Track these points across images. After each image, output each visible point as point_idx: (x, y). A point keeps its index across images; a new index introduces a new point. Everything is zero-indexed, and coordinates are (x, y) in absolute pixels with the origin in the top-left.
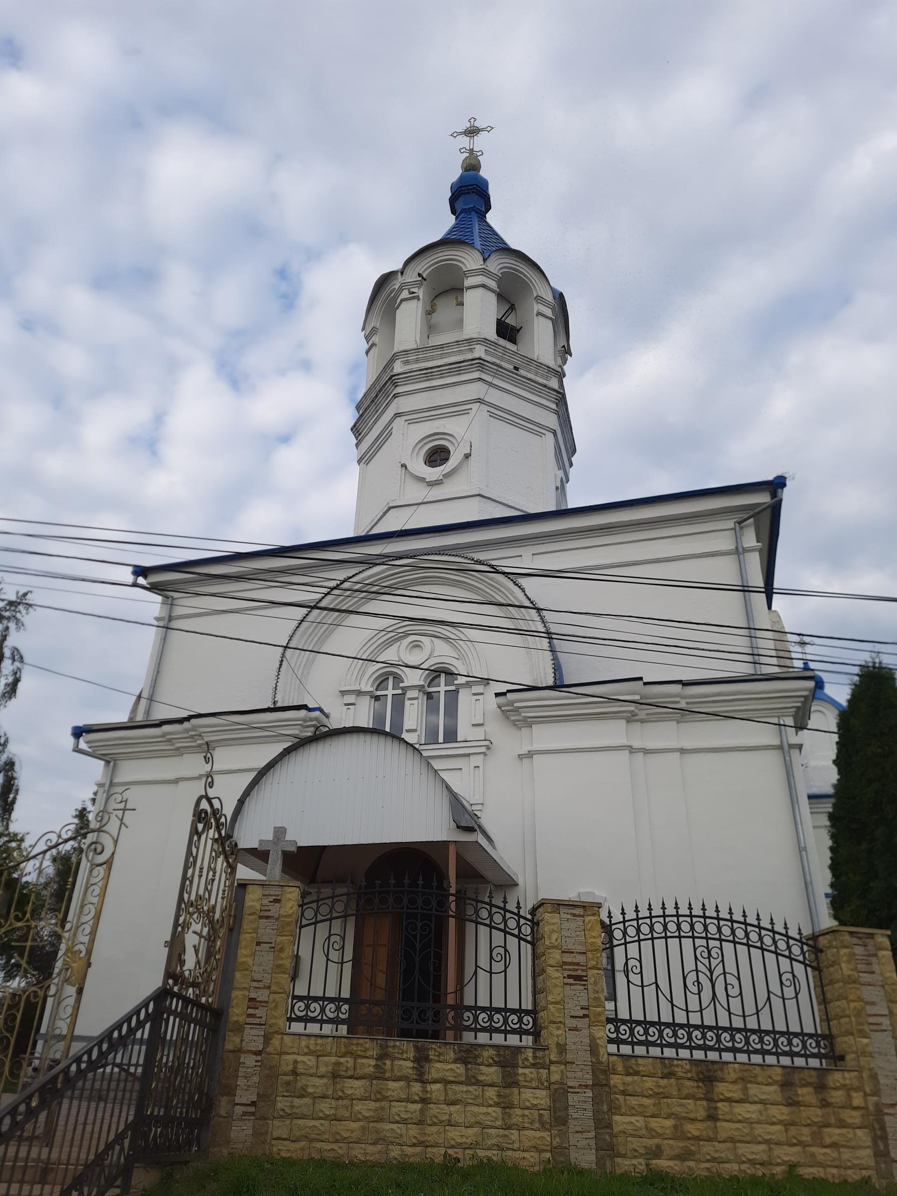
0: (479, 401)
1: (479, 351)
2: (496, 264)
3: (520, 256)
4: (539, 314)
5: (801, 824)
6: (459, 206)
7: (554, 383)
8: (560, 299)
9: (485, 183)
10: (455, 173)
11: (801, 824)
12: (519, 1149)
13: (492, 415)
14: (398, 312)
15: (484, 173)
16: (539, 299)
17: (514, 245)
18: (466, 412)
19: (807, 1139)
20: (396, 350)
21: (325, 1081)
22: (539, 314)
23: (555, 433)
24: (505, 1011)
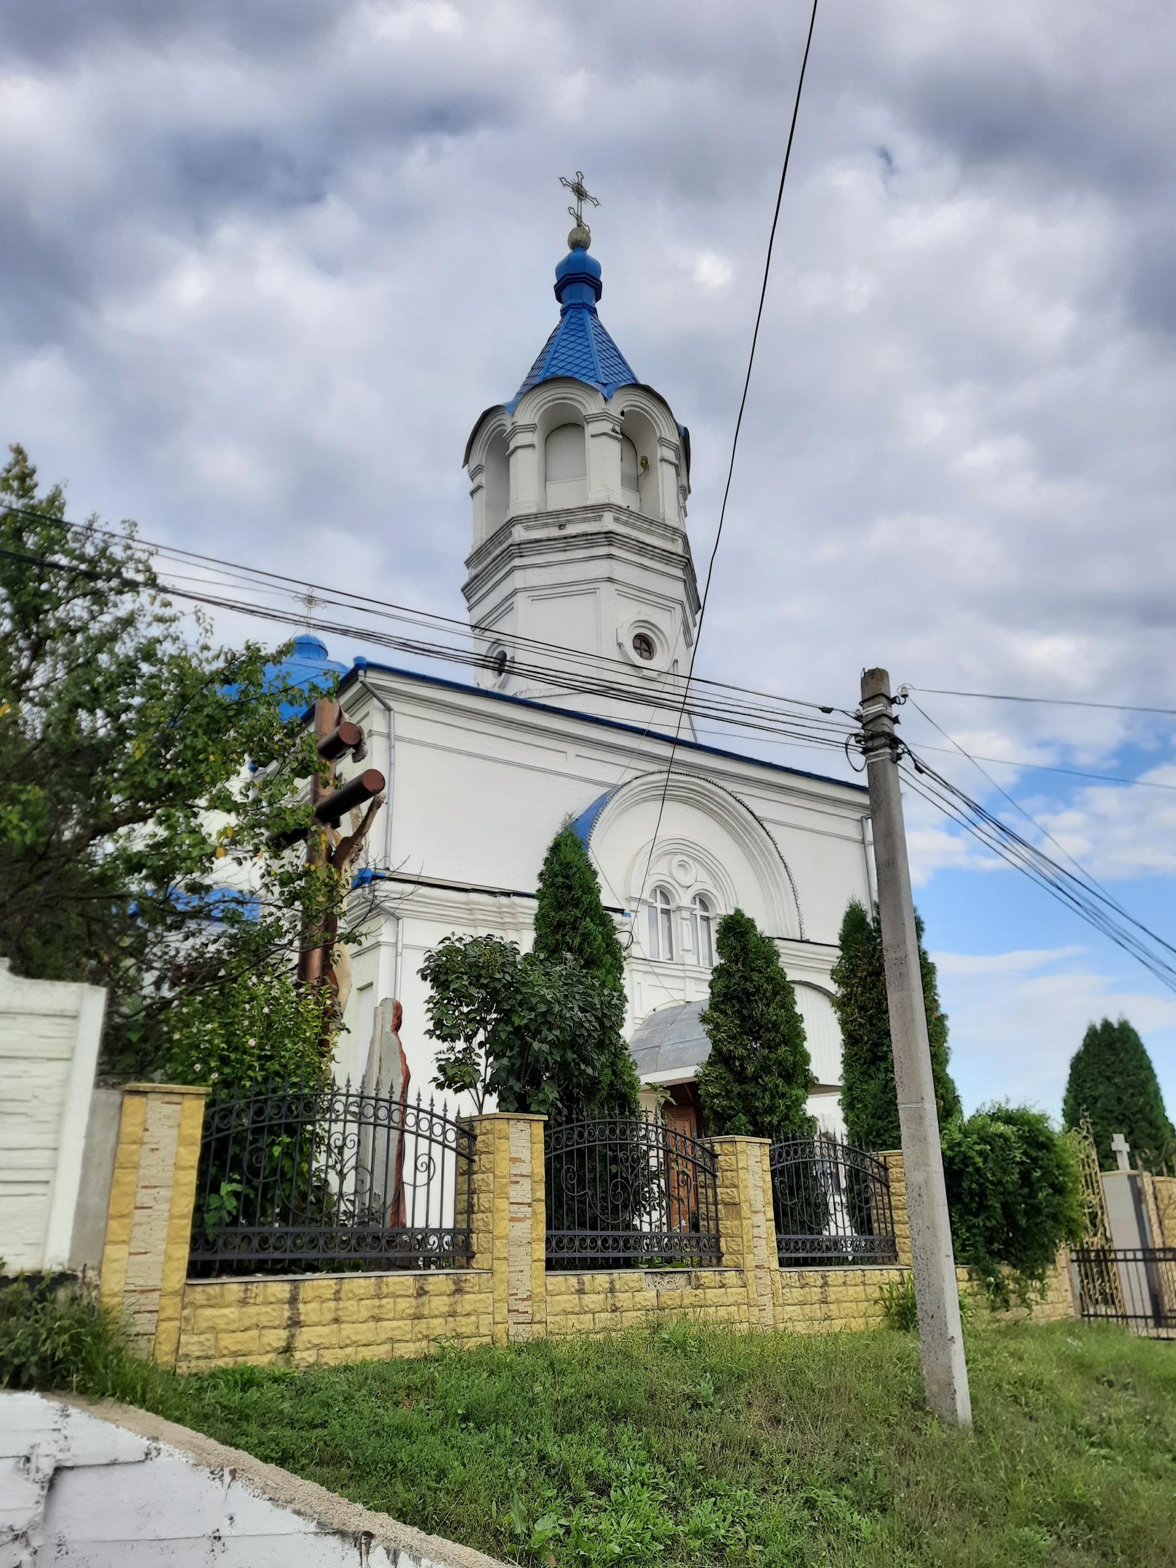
0: (610, 580)
1: (608, 522)
2: (620, 403)
3: (647, 390)
4: (663, 460)
5: (562, 563)
6: (564, 295)
7: (678, 548)
8: (685, 436)
9: (596, 268)
10: (689, 497)
11: (562, 563)
12: (394, 1319)
13: (620, 594)
14: (512, 460)
15: (593, 252)
16: (662, 441)
17: (642, 381)
18: (593, 592)
19: (260, 1079)
20: (513, 512)
21: (602, 1296)
22: (663, 460)
23: (681, 603)
24: (1126, 1260)
